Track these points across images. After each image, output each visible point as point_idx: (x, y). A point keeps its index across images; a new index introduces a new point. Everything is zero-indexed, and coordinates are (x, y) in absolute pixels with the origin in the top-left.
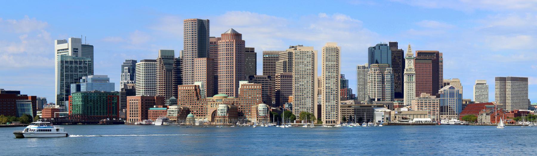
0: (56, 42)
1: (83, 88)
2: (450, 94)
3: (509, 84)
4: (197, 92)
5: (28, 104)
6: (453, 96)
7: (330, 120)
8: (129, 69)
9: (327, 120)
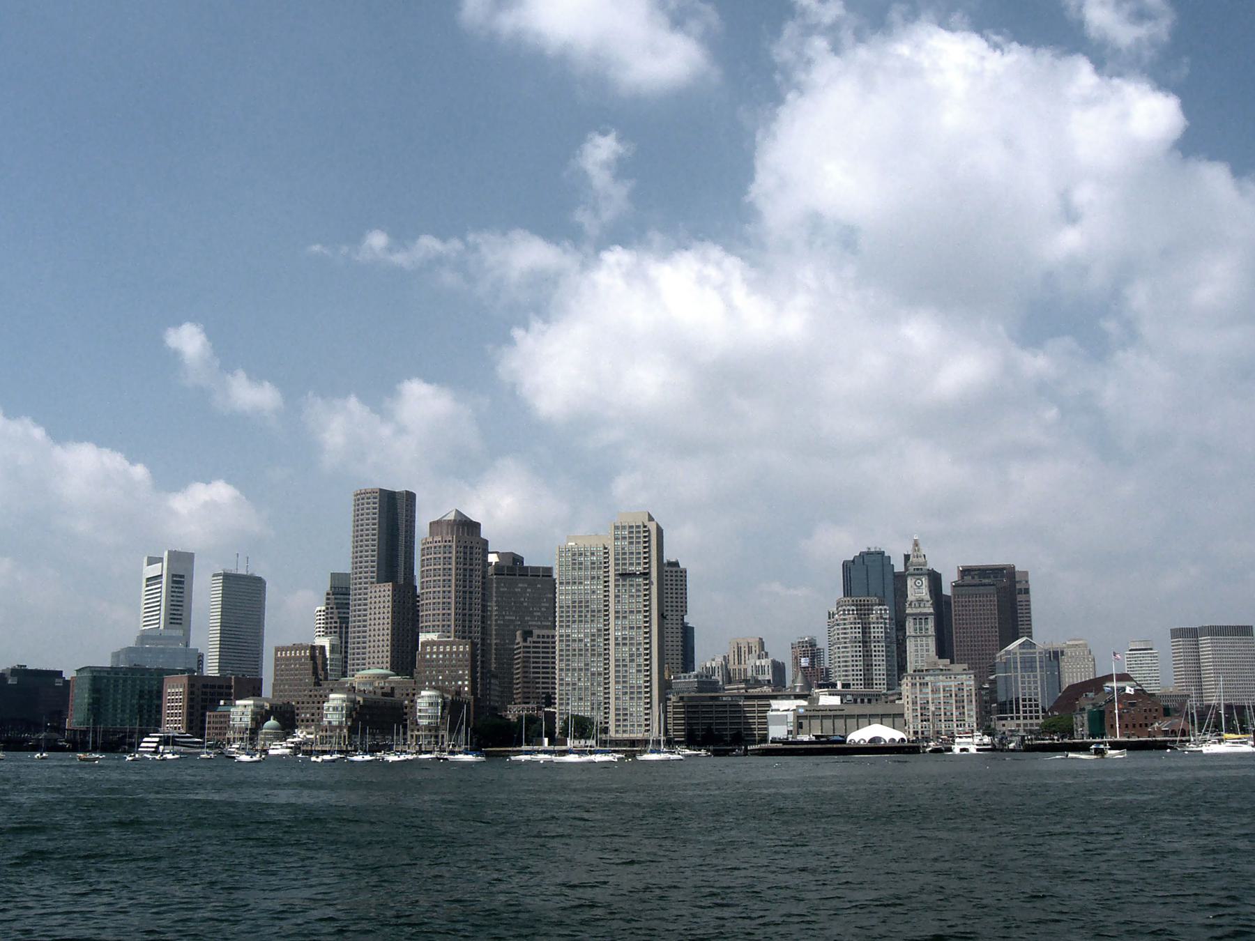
2: (1023, 661)
3: (1205, 641)
6: (1033, 669)
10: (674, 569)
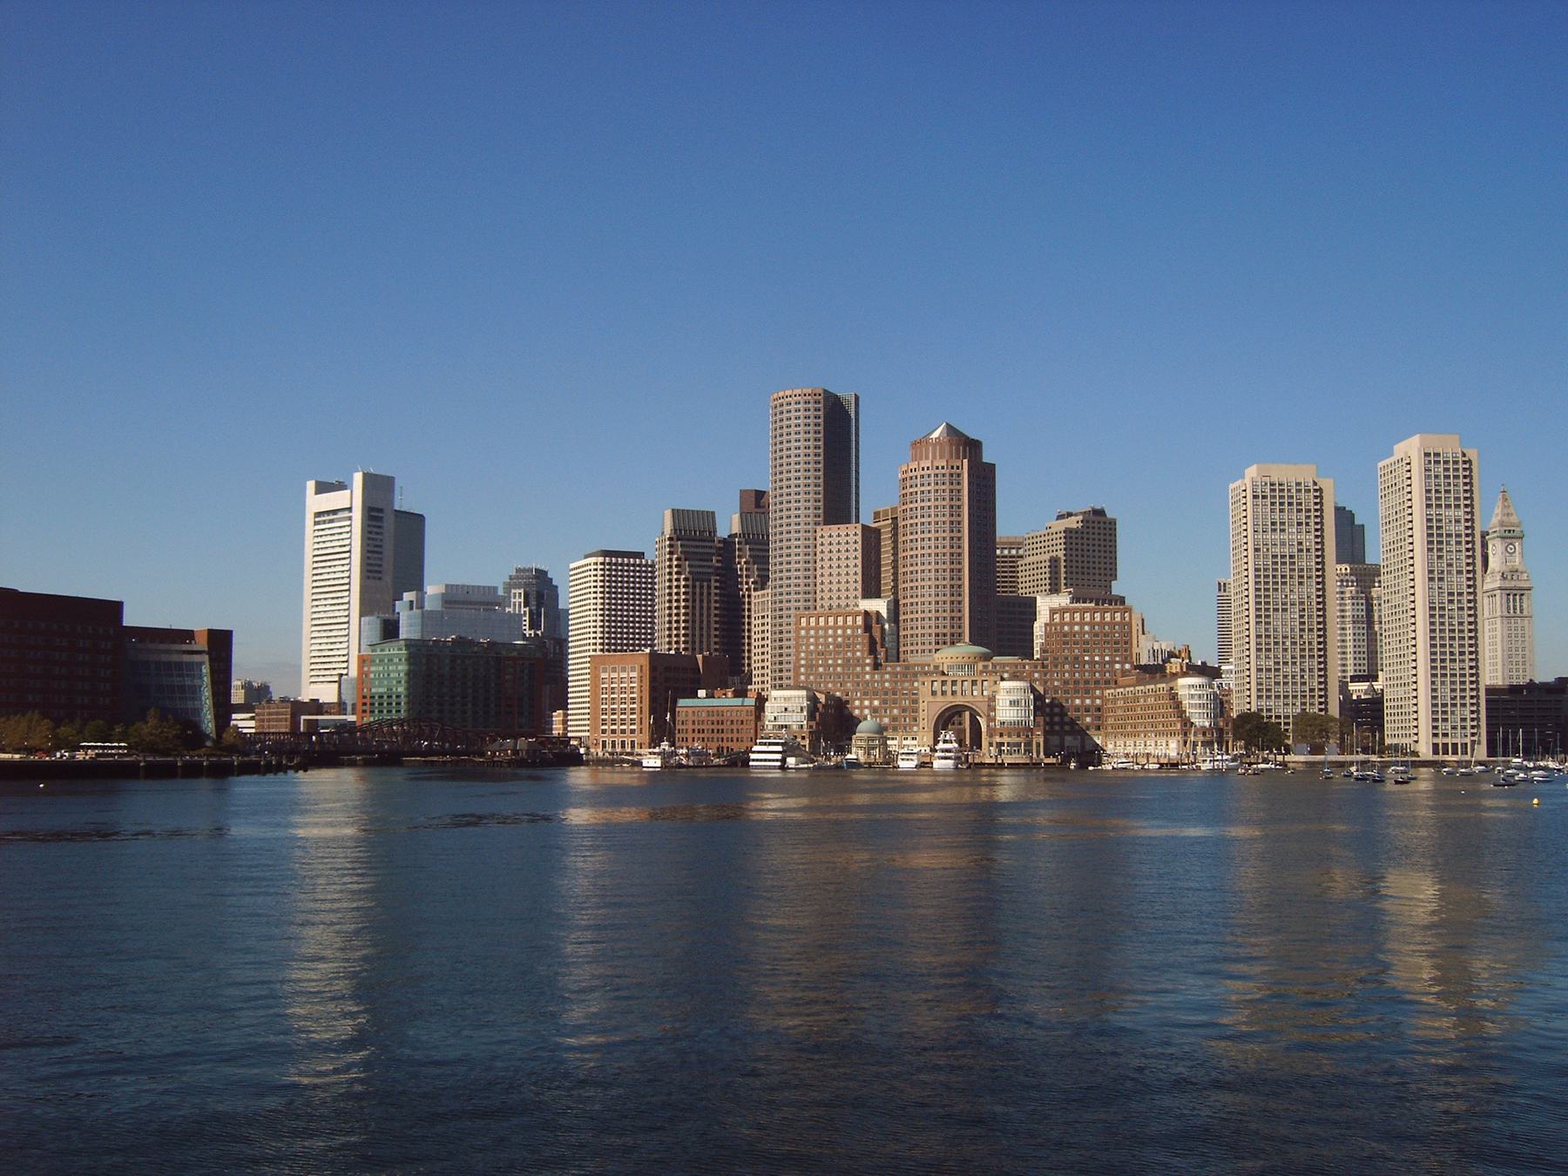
1: (408, 628)
4: (872, 639)
5: (190, 666)
7: (1448, 740)
8: (526, 595)
9: (1440, 740)
10: (1102, 519)
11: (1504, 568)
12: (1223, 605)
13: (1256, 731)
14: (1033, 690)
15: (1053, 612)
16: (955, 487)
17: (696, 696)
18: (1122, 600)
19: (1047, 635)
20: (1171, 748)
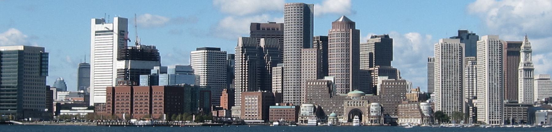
0: (93, 21)
11: (526, 62)
12: (431, 68)
13: (441, 116)
14: (380, 105)
15: (383, 81)
16: (348, 37)
17: (275, 105)
18: (395, 71)
19: (381, 88)
20: (418, 121)
